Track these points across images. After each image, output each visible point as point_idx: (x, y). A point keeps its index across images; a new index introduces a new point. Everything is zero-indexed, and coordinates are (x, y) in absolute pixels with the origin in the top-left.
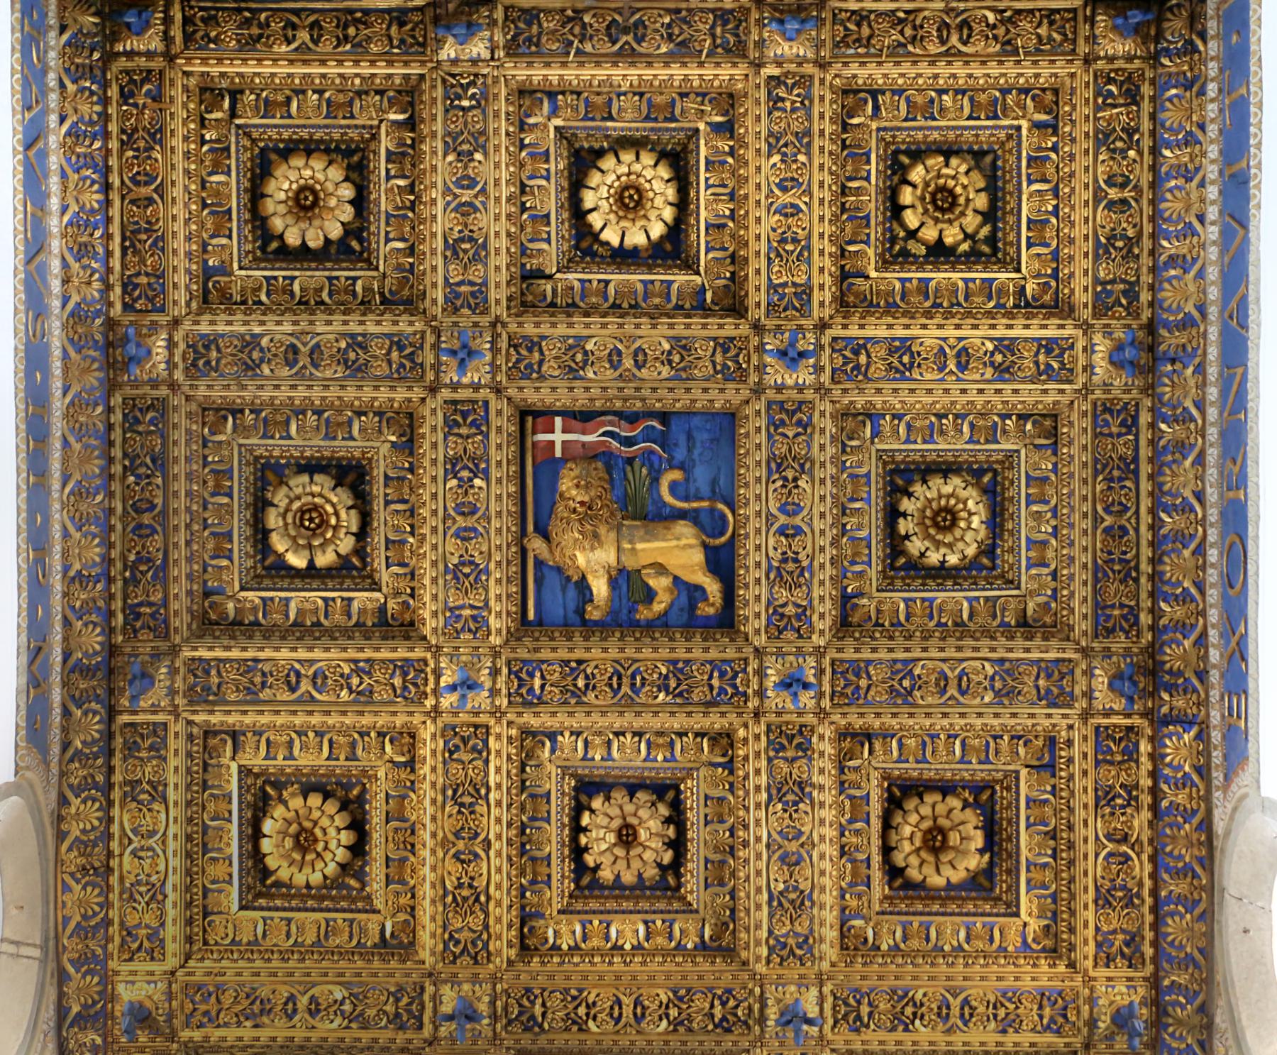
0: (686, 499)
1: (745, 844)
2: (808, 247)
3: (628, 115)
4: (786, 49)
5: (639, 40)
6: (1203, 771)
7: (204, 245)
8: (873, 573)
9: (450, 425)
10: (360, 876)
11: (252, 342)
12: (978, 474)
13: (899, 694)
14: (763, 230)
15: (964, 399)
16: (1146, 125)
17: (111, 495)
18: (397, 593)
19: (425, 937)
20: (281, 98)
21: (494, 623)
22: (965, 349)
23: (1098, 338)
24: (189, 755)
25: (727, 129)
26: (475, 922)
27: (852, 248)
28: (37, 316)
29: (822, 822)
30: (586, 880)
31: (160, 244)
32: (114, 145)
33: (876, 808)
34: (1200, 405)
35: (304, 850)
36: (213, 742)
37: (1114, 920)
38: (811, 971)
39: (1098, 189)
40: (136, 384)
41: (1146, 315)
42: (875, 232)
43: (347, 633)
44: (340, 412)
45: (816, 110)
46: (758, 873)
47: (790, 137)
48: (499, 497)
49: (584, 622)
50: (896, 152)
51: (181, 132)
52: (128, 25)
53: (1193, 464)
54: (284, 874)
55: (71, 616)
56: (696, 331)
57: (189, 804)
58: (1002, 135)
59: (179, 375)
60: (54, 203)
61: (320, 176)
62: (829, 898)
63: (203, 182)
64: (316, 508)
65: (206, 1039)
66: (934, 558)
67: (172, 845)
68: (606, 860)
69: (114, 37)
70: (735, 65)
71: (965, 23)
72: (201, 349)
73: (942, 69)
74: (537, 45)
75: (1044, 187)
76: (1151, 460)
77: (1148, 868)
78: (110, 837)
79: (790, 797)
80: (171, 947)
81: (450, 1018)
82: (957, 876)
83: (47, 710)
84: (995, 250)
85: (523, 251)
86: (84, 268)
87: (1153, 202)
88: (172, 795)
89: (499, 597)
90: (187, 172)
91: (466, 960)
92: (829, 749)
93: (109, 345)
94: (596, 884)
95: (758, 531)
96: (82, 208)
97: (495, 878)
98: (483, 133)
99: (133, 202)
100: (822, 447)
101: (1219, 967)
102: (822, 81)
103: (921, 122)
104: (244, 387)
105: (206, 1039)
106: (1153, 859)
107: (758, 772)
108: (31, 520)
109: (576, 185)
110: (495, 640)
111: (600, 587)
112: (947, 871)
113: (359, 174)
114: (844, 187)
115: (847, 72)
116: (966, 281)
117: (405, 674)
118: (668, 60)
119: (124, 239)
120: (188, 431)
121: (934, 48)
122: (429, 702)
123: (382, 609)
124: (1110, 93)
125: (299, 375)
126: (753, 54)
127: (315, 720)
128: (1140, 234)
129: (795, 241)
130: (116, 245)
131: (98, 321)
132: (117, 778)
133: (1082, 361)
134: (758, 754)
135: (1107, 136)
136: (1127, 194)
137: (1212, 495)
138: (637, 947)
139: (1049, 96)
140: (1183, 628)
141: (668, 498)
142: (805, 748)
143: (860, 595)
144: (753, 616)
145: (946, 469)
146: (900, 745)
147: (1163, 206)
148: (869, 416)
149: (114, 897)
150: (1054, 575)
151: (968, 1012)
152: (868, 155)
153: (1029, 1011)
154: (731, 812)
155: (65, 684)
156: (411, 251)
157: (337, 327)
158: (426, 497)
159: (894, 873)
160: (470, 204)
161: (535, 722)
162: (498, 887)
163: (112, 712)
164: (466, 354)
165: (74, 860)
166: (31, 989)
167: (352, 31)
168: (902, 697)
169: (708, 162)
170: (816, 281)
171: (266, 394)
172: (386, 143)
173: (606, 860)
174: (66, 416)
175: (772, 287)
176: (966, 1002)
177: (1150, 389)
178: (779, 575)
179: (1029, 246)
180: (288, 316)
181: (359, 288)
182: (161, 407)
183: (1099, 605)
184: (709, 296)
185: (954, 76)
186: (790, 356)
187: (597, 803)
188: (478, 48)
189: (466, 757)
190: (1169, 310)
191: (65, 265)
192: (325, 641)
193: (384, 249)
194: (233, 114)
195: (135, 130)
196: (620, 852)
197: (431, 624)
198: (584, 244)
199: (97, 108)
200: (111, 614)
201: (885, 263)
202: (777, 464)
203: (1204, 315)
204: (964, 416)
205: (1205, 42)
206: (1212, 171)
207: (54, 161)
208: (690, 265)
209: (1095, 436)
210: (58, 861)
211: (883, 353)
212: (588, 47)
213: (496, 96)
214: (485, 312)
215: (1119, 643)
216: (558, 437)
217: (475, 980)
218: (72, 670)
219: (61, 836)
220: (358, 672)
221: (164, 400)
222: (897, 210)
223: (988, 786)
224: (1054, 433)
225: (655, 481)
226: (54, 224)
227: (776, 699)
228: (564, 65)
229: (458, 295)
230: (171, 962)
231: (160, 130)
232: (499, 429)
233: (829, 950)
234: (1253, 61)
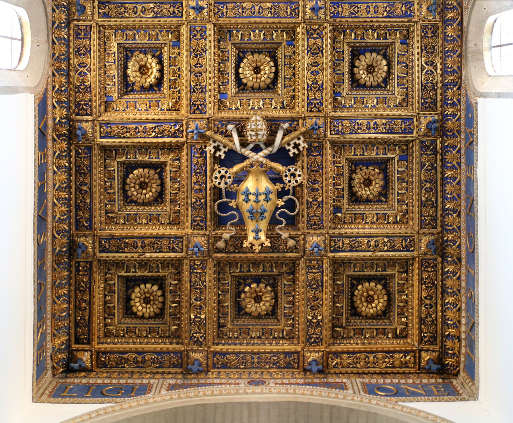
41: (73, 263)
53: (56, 249)
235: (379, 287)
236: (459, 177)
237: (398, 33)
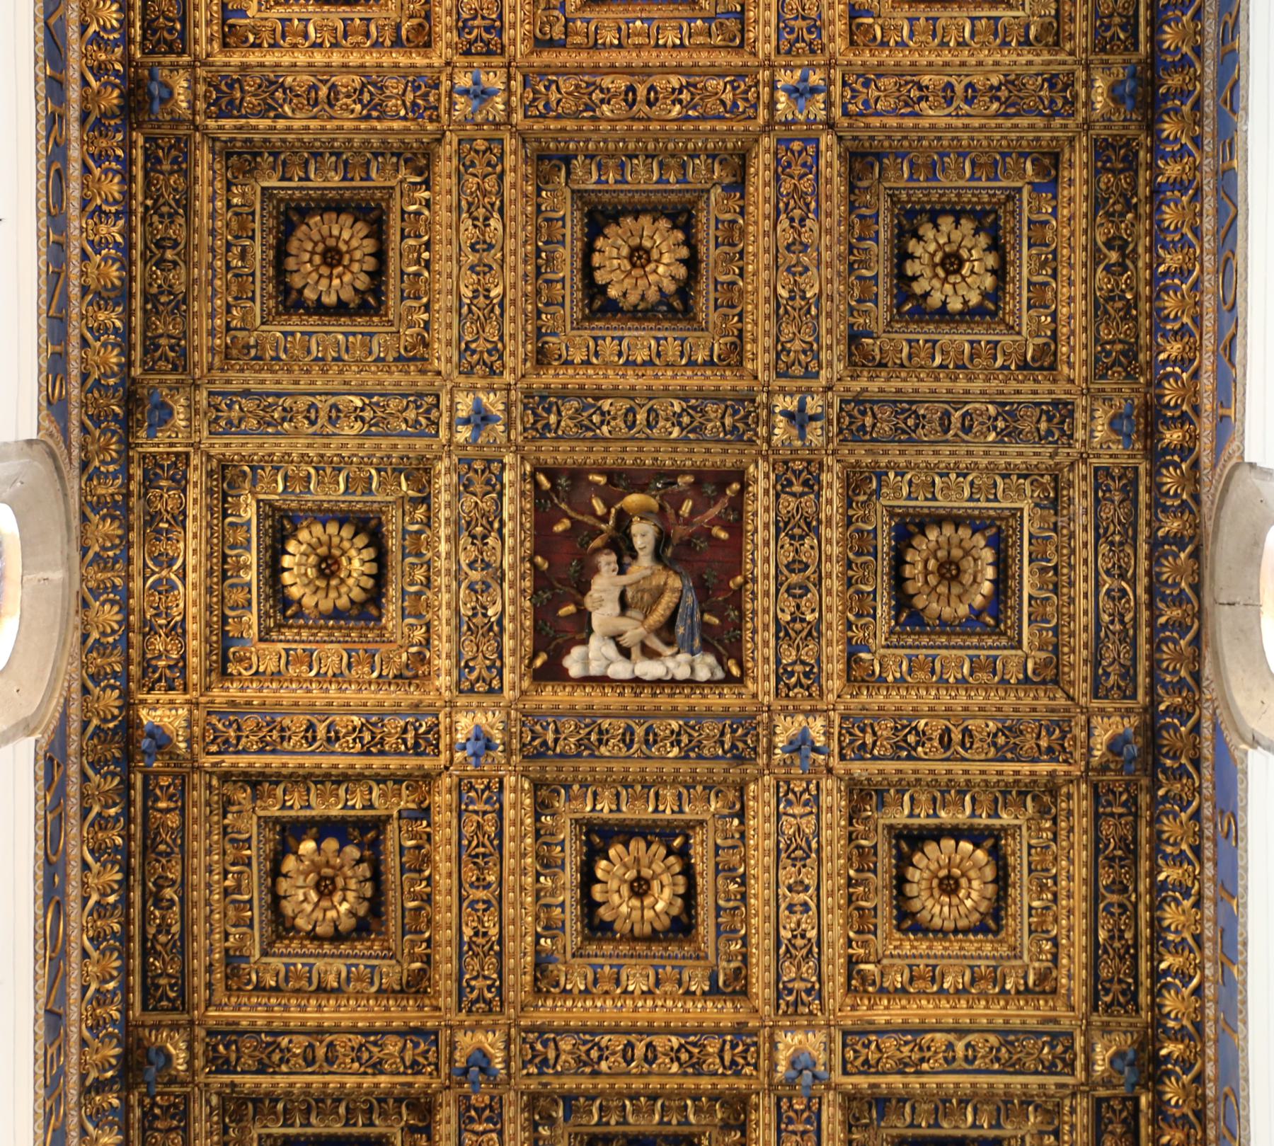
13: (374, 84)
30: (682, 219)
33: (884, 543)
235: (980, 854)
236: (1196, 626)
237: (1029, 799)
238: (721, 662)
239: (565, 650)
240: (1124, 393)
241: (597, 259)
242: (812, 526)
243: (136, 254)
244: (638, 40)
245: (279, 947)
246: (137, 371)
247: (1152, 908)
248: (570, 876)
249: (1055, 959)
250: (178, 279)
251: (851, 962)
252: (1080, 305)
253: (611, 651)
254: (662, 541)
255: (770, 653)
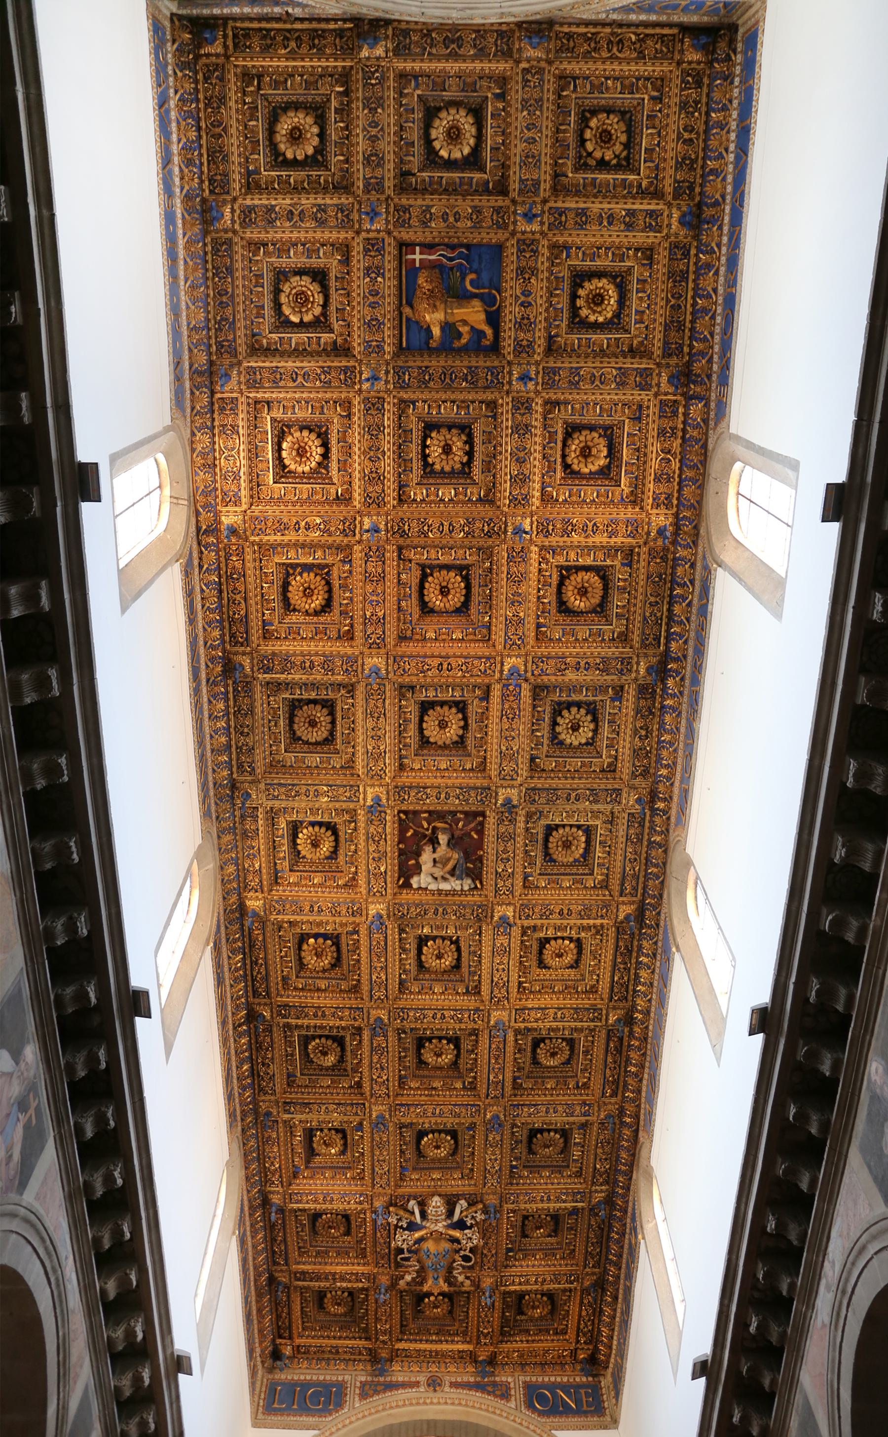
0: (478, 288)
1: (501, 453)
2: (539, 160)
3: (454, 88)
4: (531, 53)
5: (459, 47)
6: (706, 421)
7: (247, 159)
8: (564, 325)
9: (366, 251)
10: (326, 468)
11: (270, 209)
12: (614, 278)
14: (518, 150)
15: (610, 240)
16: (704, 100)
17: (207, 287)
18: (341, 335)
19: (356, 495)
20: (282, 79)
21: (386, 348)
22: (612, 214)
23: (674, 210)
24: (248, 412)
25: (501, 97)
26: (378, 489)
27: (560, 161)
28: (169, 197)
29: (535, 443)
30: (428, 470)
31: (226, 158)
32: (201, 106)
33: (560, 437)
34: (719, 245)
35: (301, 456)
36: (258, 406)
37: (663, 488)
38: (528, 510)
39: (679, 133)
40: (217, 231)
41: (697, 199)
42: (572, 153)
43: (319, 354)
44: (313, 244)
45: (546, 87)
46: (506, 466)
47: (532, 102)
48: (389, 287)
49: (429, 348)
50: (584, 111)
51: (234, 98)
52: (206, 39)
54: (292, 467)
55: (192, 347)
56: (484, 203)
57: (249, 435)
58: (635, 103)
59: (237, 227)
60: (174, 137)
61: (302, 121)
62: (537, 478)
63: (246, 125)
64: (303, 292)
65: (261, 540)
66: (592, 318)
67: (242, 454)
68: (437, 460)
69: (199, 46)
70: (506, 62)
71: (621, 41)
72: (247, 212)
73: (608, 66)
74: (409, 49)
75: (654, 131)
76: (694, 272)
77: (678, 465)
78: (215, 450)
79: (522, 432)
80: (244, 500)
81: (368, 531)
82: (594, 468)
83: (183, 392)
84: (629, 164)
85: (402, 161)
86: (190, 171)
87: (705, 141)
88: (241, 431)
89: (389, 336)
90: (237, 120)
91: (374, 505)
92: (540, 409)
93: (204, 211)
94: (433, 472)
95: (511, 304)
96: (188, 140)
97: (387, 468)
98: (382, 98)
99: (212, 136)
100: (543, 263)
101: (704, 509)
102: (549, 71)
103: (596, 95)
104: (268, 232)
105: (261, 540)
106: (680, 461)
107: (507, 420)
108: (171, 300)
109: (427, 126)
110: (388, 357)
111: (436, 331)
112: (590, 466)
113: (321, 121)
114: (558, 129)
115: (562, 67)
116: (614, 179)
117: (346, 373)
118: (474, 58)
119: (208, 156)
120: (242, 255)
121: (605, 54)
122: (357, 387)
123: (335, 342)
124: (688, 82)
125: (294, 226)
126: (516, 56)
127: (305, 395)
128: (697, 157)
129: (533, 157)
130: (205, 159)
131: (198, 199)
132: (216, 423)
133: (666, 222)
134: (507, 412)
135: (685, 104)
136: (693, 136)
137: (721, 290)
138: (451, 500)
139: (659, 82)
140: (702, 354)
141: (469, 287)
142: (529, 409)
143: (557, 336)
144: (508, 346)
145: (599, 274)
146: (572, 408)
147: (710, 142)
148: (565, 247)
149: (218, 478)
150: (647, 327)
151: (595, 529)
152: (570, 112)
153: (622, 528)
154: (495, 438)
155: (191, 379)
156: (347, 161)
157: (312, 201)
158: (355, 287)
159: (566, 466)
160: (375, 136)
161: (405, 396)
162: (389, 472)
163: (213, 393)
164: (373, 215)
165: (199, 461)
166: (185, 518)
167: (316, 41)
168: (574, 385)
169: (492, 115)
170: (542, 178)
171: (278, 236)
172: (334, 104)
173: (437, 460)
174: (185, 248)
175: (521, 181)
176: (595, 524)
177: (696, 237)
178: (520, 326)
179: (645, 162)
180: (288, 196)
181: (322, 181)
182: (229, 243)
183: (666, 343)
184: (491, 185)
185: (613, 70)
186: (529, 217)
187: (433, 435)
188: (379, 51)
189: (374, 413)
190: (708, 197)
191: (181, 170)
192: (309, 358)
193: (334, 160)
194: (259, 88)
195: (212, 97)
196: (444, 457)
197: (357, 349)
198: (431, 158)
199: (193, 86)
200: (210, 346)
201: (576, 170)
202: (521, 271)
203: (724, 200)
204: (609, 249)
205: (735, 55)
206: (733, 125)
207: (173, 115)
208: (482, 169)
209: (670, 259)
210: (193, 462)
211: (573, 216)
212: (434, 51)
213: (388, 78)
214: (383, 193)
215: (674, 361)
216: (417, 257)
217: (378, 514)
218: (194, 372)
219: (193, 450)
220: (324, 372)
221: (231, 239)
222: (582, 141)
223: (611, 427)
224: (650, 258)
225: (463, 279)
226: (175, 149)
227: (517, 385)
228: (422, 61)
229: (369, 184)
230: (244, 507)
231: (224, 97)
232: (389, 253)
233: (536, 502)
234: (757, 65)
238: (473, 881)
239: (412, 876)
240: (643, 784)
241: (425, 725)
242: (512, 837)
243: (232, 730)
244: (444, 637)
245: (302, 974)
246: (235, 776)
247: (636, 969)
248: (413, 953)
249: (598, 981)
250: (250, 741)
251: (520, 983)
252: (627, 752)
253: (430, 879)
254: (452, 838)
255: (493, 883)
